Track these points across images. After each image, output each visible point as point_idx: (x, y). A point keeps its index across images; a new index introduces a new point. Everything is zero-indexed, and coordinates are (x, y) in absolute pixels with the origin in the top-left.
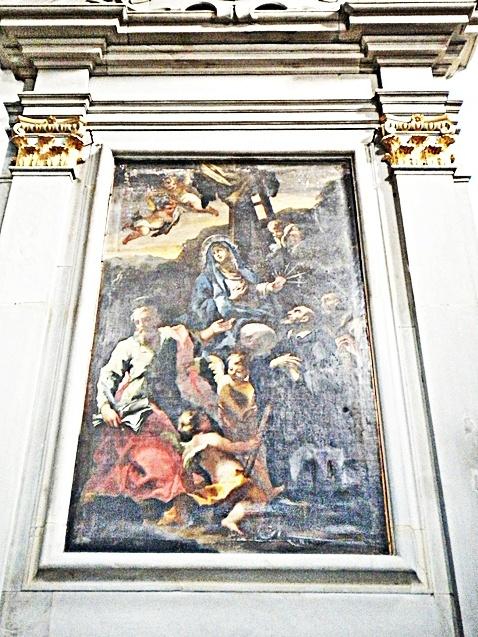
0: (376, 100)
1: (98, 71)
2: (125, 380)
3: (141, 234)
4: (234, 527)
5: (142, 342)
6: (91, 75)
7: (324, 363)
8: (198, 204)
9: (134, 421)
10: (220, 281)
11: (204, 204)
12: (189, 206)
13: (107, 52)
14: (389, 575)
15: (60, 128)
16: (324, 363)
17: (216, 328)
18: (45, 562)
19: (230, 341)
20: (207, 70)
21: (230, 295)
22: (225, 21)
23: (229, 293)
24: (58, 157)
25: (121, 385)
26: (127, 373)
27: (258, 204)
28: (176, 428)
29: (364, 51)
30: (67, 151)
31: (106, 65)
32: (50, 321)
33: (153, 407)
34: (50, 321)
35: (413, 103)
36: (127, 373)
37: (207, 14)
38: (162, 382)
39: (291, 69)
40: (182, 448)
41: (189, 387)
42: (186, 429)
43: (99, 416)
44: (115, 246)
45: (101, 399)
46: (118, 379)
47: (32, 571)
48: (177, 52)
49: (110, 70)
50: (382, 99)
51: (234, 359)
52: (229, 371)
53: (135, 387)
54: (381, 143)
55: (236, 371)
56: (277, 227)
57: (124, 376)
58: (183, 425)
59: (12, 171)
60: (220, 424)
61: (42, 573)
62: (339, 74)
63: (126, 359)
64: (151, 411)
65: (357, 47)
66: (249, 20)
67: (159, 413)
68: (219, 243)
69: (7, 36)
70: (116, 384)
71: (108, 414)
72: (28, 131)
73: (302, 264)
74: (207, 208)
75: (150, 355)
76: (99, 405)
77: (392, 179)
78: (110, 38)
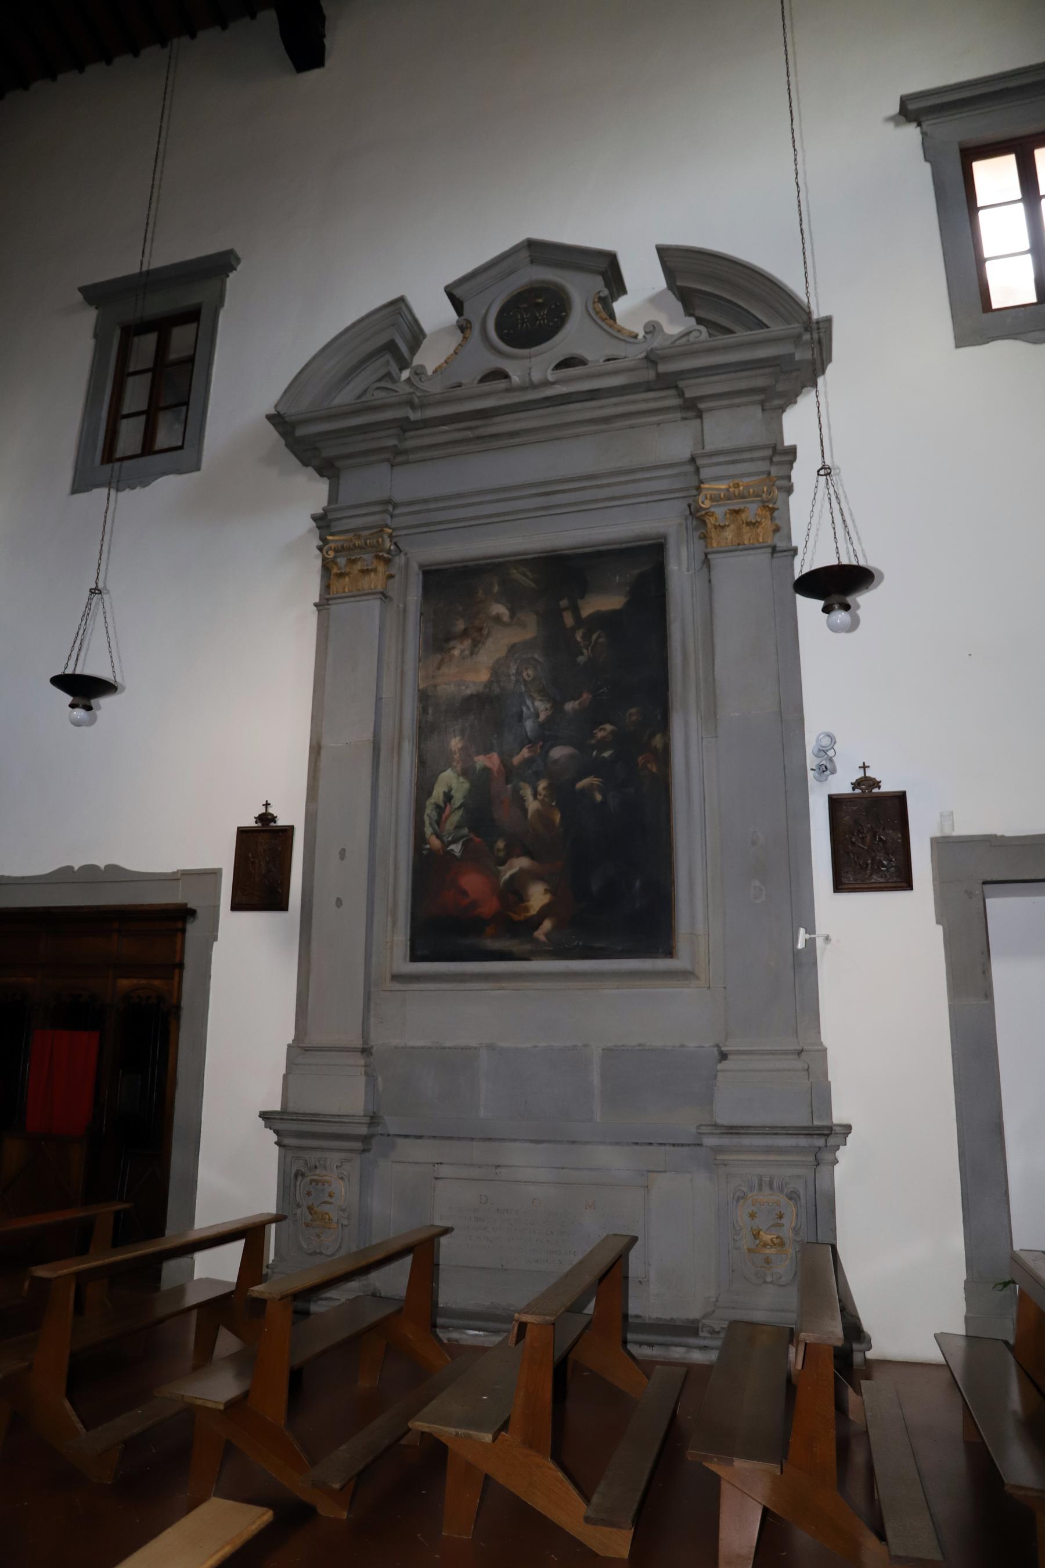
0: (693, 460)
1: (399, 459)
2: (448, 811)
4: (543, 938)
6: (392, 466)
8: (506, 618)
9: (456, 848)
10: (529, 703)
11: (512, 616)
12: (497, 619)
13: (405, 439)
15: (366, 543)
17: (525, 753)
18: (395, 971)
20: (512, 441)
22: (522, 389)
23: (537, 715)
24: (367, 578)
25: (444, 816)
27: (566, 609)
29: (681, 394)
30: (375, 570)
31: (405, 452)
32: (159, 142)
33: (472, 835)
34: (159, 142)
35: (734, 462)
37: (502, 384)
38: (479, 814)
39: (605, 427)
40: (499, 872)
42: (501, 854)
43: (428, 846)
45: (428, 830)
46: (439, 809)
47: (388, 977)
48: (477, 427)
49: (411, 457)
50: (699, 462)
51: (542, 785)
52: (539, 797)
53: (455, 818)
54: (698, 517)
56: (584, 637)
58: (499, 850)
59: (328, 600)
61: (396, 977)
62: (659, 424)
63: (446, 790)
64: (471, 839)
65: (673, 392)
66: (547, 384)
67: (477, 839)
70: (440, 815)
71: (435, 842)
72: (336, 551)
75: (467, 785)
76: (427, 836)
77: (706, 562)
78: (405, 426)
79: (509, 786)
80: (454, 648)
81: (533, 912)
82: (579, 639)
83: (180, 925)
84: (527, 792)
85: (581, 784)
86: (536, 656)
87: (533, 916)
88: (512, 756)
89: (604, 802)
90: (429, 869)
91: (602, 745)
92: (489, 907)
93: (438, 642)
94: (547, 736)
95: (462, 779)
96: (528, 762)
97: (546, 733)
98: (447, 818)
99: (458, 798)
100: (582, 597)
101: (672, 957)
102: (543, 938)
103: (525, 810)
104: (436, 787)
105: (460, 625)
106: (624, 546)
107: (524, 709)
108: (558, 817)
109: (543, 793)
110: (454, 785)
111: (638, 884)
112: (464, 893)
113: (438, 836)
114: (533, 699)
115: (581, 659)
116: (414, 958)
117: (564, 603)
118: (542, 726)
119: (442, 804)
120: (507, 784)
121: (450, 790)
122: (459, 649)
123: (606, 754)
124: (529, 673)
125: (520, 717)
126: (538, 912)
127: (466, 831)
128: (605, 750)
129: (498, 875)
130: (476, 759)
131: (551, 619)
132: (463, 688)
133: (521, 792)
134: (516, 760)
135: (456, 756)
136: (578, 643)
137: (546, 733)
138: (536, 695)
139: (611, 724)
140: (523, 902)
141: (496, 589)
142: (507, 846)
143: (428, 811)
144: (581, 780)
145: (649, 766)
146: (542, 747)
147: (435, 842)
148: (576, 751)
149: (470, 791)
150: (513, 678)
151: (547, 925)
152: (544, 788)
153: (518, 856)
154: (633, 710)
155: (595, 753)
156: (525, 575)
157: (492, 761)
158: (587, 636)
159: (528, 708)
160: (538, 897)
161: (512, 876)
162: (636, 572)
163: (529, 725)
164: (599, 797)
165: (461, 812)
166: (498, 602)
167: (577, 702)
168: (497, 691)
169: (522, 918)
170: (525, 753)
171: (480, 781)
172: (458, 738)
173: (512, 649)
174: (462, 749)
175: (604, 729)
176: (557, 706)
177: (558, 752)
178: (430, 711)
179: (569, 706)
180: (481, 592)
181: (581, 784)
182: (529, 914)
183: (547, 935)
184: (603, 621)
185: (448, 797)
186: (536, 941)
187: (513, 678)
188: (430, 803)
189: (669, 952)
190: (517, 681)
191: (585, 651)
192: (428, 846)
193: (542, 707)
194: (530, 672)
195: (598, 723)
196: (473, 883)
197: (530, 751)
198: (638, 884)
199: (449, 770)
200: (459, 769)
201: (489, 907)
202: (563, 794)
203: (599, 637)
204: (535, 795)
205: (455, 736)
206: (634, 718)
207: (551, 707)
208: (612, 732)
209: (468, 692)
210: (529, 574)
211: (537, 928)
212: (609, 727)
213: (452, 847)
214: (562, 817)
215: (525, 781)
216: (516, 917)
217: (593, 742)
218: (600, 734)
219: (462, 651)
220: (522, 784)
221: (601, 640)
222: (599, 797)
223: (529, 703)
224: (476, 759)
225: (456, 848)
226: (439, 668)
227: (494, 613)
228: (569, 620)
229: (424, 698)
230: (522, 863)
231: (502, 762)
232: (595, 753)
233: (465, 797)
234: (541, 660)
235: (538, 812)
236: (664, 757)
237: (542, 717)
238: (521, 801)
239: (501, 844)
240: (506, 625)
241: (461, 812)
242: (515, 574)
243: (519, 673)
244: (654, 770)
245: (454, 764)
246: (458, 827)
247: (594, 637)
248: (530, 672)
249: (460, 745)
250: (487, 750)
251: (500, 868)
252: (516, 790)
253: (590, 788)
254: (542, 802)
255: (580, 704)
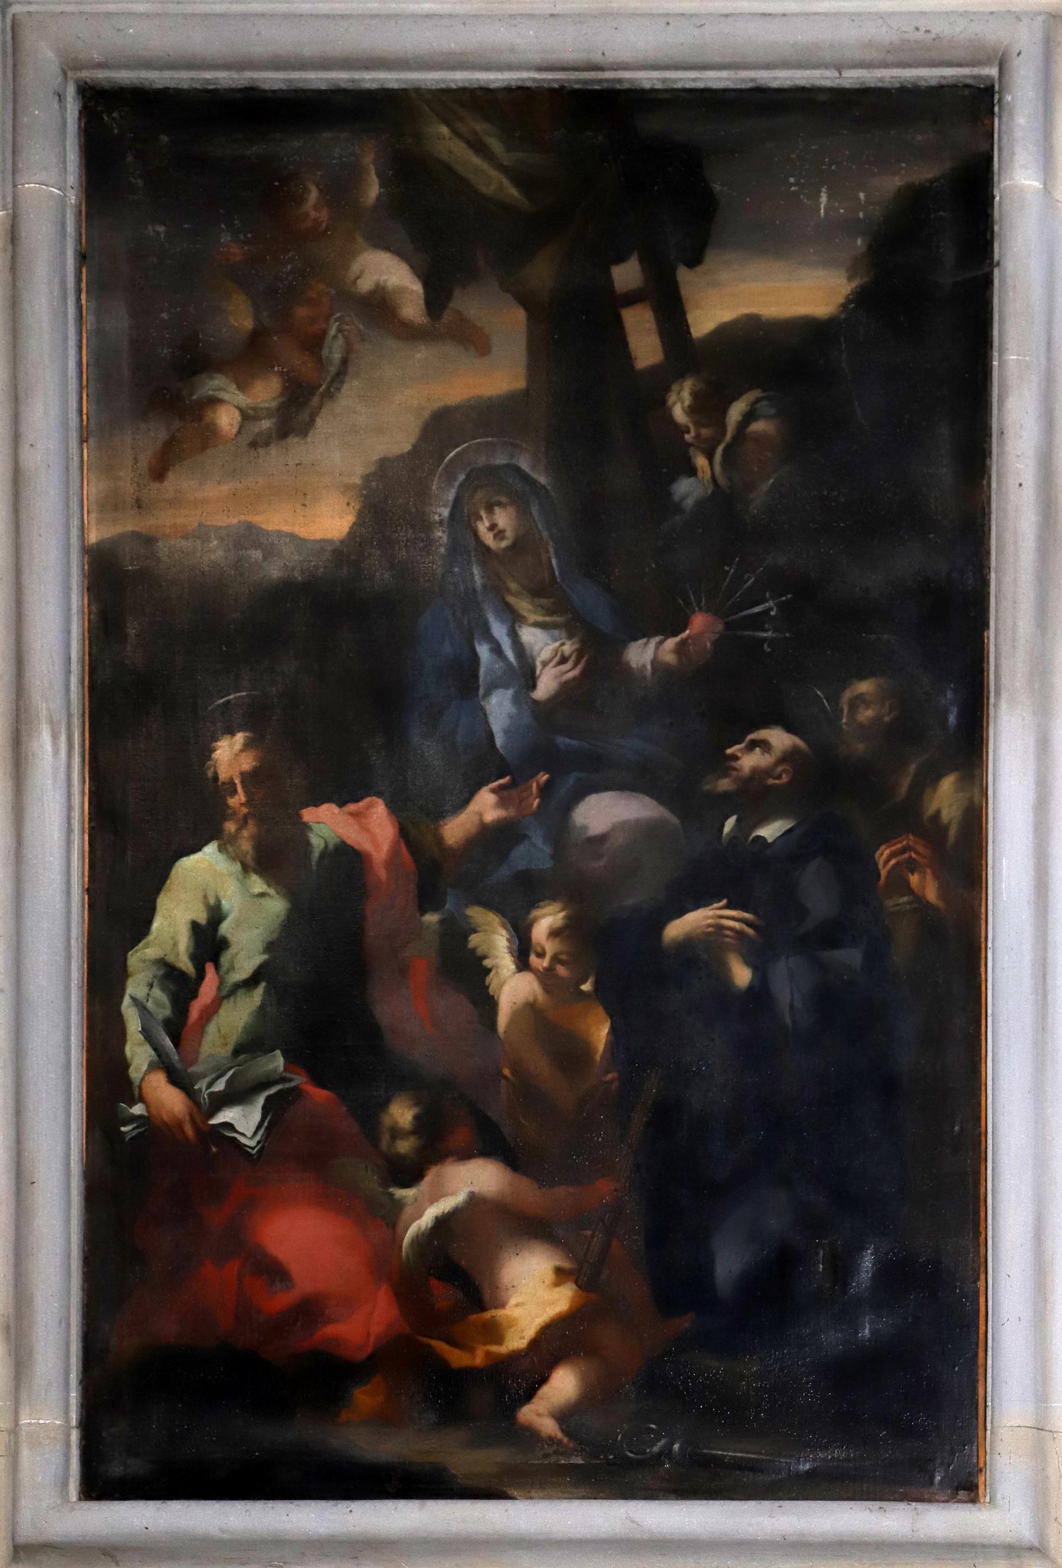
2: (208, 989)
3: (209, 436)
4: (549, 1426)
5: (249, 860)
7: (831, 935)
8: (412, 306)
9: (244, 1120)
10: (499, 630)
11: (436, 299)
12: (379, 307)
14: (730, 19)
16: (831, 935)
17: (486, 806)
18: (27, 1532)
19: (534, 853)
21: (533, 686)
23: (531, 680)
25: (195, 1009)
26: (210, 968)
27: (632, 299)
28: (375, 1142)
33: (299, 1080)
36: (210, 968)
38: (326, 1002)
40: (398, 1206)
41: (409, 1013)
42: (405, 1146)
43: (138, 1109)
44: (128, 487)
45: (139, 1055)
46: (180, 985)
51: (546, 921)
52: (533, 959)
53: (237, 1017)
55: (555, 959)
57: (201, 975)
58: (396, 1133)
60: (506, 1131)
63: (202, 918)
64: (295, 1094)
68: (491, 471)
69: (219, 1031)
71: (168, 1099)
73: (782, 560)
74: (447, 316)
75: (277, 906)
79: (432, 918)
80: (214, 402)
81: (517, 1340)
82: (679, 414)
83: (414, 95)
84: (496, 943)
85: (676, 929)
86: (524, 464)
87: (515, 1356)
88: (439, 815)
89: (759, 994)
90: (141, 1186)
91: (756, 798)
92: (365, 1322)
93: (149, 387)
94: (562, 752)
95: (257, 884)
96: (496, 839)
97: (562, 741)
98: (210, 1012)
99: (246, 953)
100: (694, 260)
101: (974, 1500)
102: (549, 1426)
103: (488, 1004)
104: (164, 902)
105: (240, 317)
106: (851, 78)
107: (483, 651)
108: (600, 1033)
109: (551, 947)
110: (232, 899)
111: (867, 1262)
112: (274, 1271)
113: (177, 1078)
114: (514, 619)
115: (687, 490)
116: (97, 1486)
117: (627, 274)
118: (545, 715)
119: (186, 964)
120: (423, 911)
121: (216, 915)
122: (232, 405)
123: (770, 831)
124: (498, 524)
125: (466, 679)
126: (534, 1343)
127: (277, 1062)
128: (764, 819)
129: (391, 1215)
130: (308, 815)
131: (576, 333)
132: (256, 554)
133: (474, 940)
134: (455, 829)
135: (237, 800)
136: (683, 430)
137: (562, 741)
138: (523, 606)
139: (789, 729)
140: (483, 1308)
141: (373, 191)
142: (421, 1125)
143: (136, 987)
144: (681, 912)
145: (914, 879)
146: (545, 791)
147: (168, 1099)
148: (674, 820)
149: (289, 925)
150: (441, 535)
151: (564, 1384)
152: (554, 933)
153: (465, 1156)
154: (865, 687)
155: (730, 824)
156: (479, 147)
157: (363, 826)
158: (710, 406)
159: (497, 649)
160: (532, 1291)
161: (442, 1223)
162: (890, 183)
163: (500, 709)
164: (742, 975)
165: (258, 995)
166: (381, 243)
167: (671, 643)
168: (383, 577)
169: (478, 1359)
170: (486, 806)
171: (328, 904)
172: (240, 738)
173: (441, 428)
174: (250, 779)
175: (764, 745)
176: (599, 652)
177: (603, 813)
178: (132, 630)
179: (642, 654)
180: (314, 195)
181: (676, 929)
182: (504, 1349)
183: (564, 1416)
184: (766, 355)
185: (209, 941)
186: (529, 1436)
187: (441, 535)
188: (141, 959)
189: (967, 1486)
190: (455, 548)
191: (701, 461)
192: (138, 1109)
193: (548, 651)
194: (504, 518)
195: (740, 723)
196: (304, 1239)
197: (502, 803)
198: (867, 1262)
199: (210, 849)
200: (246, 845)
201: (365, 1322)
202: (618, 954)
203: (750, 416)
204: (523, 953)
205: (231, 732)
206: (866, 714)
207: (580, 653)
208: (789, 757)
209: (274, 572)
210: (496, 145)
211: (529, 1395)
212: (779, 739)
213: (227, 1115)
214: (613, 1030)
215: (487, 905)
216: (458, 1358)
217: (725, 784)
218: (750, 761)
219: (247, 416)
220: (477, 914)
221: (758, 426)
222: (742, 975)
223: (499, 630)
224: (308, 815)
225: (244, 1120)
226: (158, 473)
227: (365, 285)
228: (644, 341)
229: (114, 584)
230: (472, 1179)
231: (404, 832)
232: (730, 824)
233: (270, 947)
234: (542, 480)
235: (531, 1008)
236: (964, 856)
237: (546, 686)
238: (469, 974)
239: (402, 1113)
240: (411, 334)
241: (258, 995)
242: (445, 142)
243: (462, 520)
244: (931, 894)
245: (230, 827)
246: (250, 1046)
247: (736, 411)
248: (504, 518)
249: (247, 763)
250: (346, 790)
251: (400, 1193)
252: (456, 933)
253: (712, 941)
254: (546, 978)
255: (680, 649)
